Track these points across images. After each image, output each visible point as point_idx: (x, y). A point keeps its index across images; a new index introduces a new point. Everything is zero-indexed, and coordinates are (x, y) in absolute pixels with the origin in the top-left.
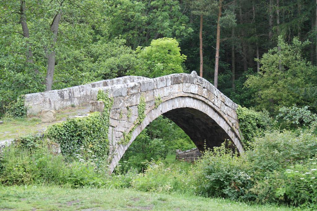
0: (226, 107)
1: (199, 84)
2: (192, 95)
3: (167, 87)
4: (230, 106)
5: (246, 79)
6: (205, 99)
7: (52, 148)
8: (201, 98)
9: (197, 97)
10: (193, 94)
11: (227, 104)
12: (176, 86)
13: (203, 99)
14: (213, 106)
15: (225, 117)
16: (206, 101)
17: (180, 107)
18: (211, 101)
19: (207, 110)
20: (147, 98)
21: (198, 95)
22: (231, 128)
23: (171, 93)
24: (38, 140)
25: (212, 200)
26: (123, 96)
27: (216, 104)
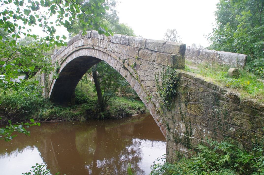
1: (83, 37)
2: (82, 47)
3: (66, 49)
4: (117, 42)
5: (89, 2)
6: (91, 46)
7: (120, 82)
8: (88, 47)
9: (85, 47)
11: (114, 42)
14: (99, 49)
17: (94, 57)
18: (96, 45)
19: (96, 54)
20: (59, 58)
21: (85, 45)
23: (69, 51)
24: (239, 82)
25: (143, 151)
26: (24, 62)
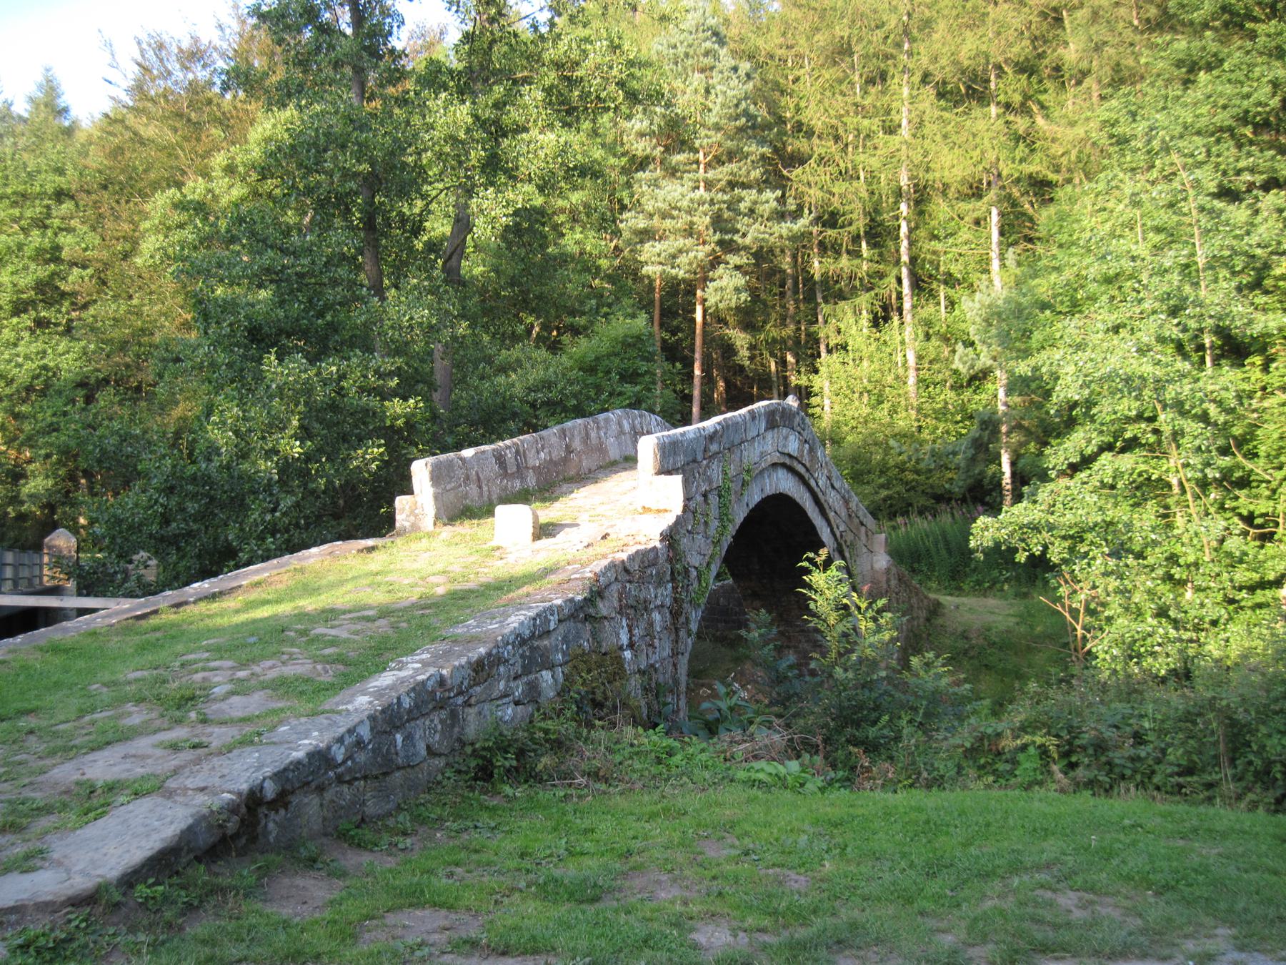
0: (833, 493)
2: (788, 461)
10: (790, 456)
12: (769, 435)
13: (802, 470)
15: (831, 515)
16: (807, 476)
22: (839, 545)
27: (820, 483)
